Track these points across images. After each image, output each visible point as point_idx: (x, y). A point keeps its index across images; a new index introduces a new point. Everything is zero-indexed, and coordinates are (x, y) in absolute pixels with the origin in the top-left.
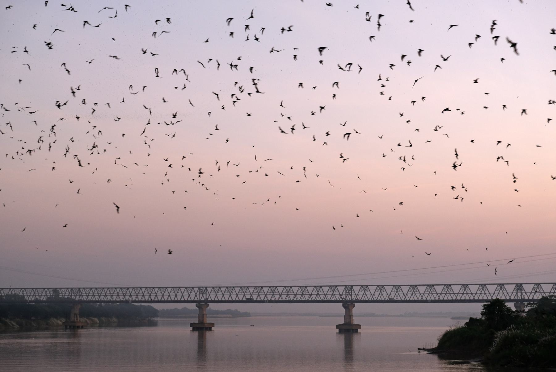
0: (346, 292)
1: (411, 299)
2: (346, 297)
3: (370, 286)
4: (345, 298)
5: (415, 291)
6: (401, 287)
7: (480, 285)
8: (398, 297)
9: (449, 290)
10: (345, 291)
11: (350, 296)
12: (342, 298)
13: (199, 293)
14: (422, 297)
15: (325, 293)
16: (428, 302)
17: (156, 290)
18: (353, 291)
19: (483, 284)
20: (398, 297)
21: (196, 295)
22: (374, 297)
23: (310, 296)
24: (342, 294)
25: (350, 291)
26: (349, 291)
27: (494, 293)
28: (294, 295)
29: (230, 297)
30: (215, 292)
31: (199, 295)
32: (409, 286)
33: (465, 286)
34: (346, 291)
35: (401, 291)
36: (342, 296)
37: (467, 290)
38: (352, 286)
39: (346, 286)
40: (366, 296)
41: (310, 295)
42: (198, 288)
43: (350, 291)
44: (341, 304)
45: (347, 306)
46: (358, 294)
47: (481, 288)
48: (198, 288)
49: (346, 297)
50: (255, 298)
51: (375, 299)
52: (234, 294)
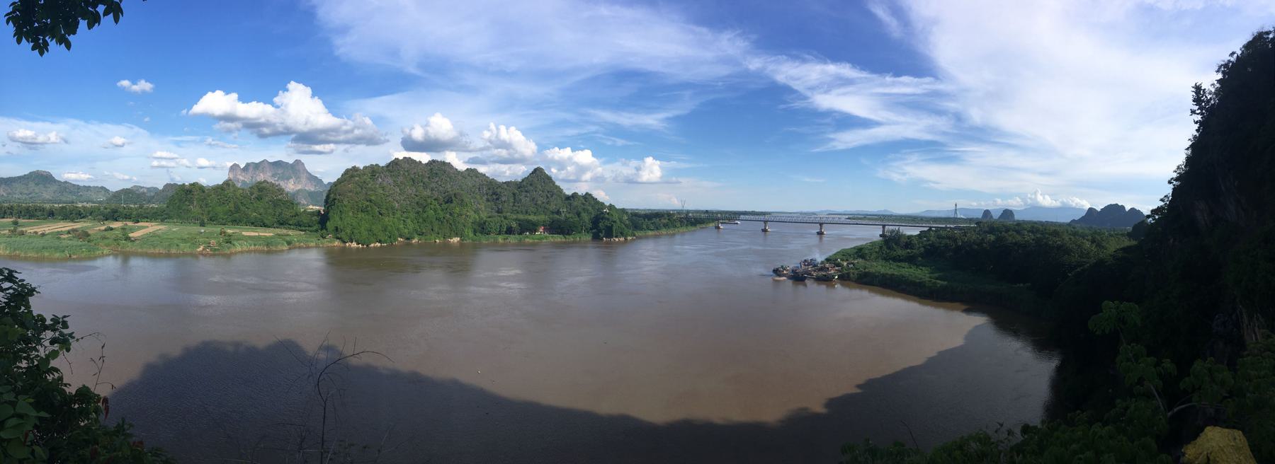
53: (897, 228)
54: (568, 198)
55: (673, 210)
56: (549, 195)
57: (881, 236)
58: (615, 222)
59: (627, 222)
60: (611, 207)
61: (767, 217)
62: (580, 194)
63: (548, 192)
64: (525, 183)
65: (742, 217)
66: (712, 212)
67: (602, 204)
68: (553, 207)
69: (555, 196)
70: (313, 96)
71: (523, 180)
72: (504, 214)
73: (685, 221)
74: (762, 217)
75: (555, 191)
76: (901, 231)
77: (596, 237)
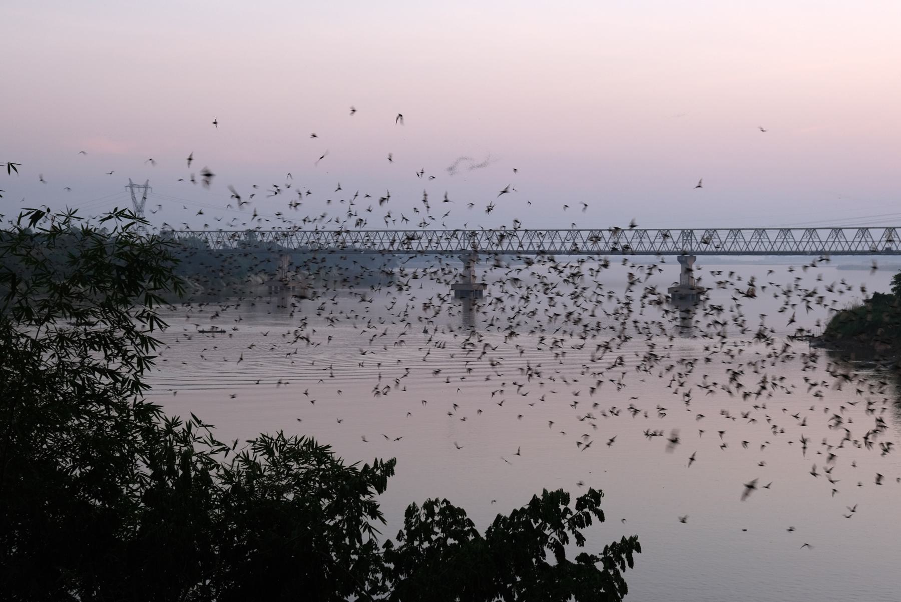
0: (683, 240)
1: (781, 250)
2: (683, 246)
3: (671, 230)
4: (681, 247)
5: (813, 237)
6: (869, 230)
7: (807, 229)
8: (762, 247)
9: (839, 237)
10: (681, 238)
11: (689, 246)
12: (677, 248)
13: (464, 239)
14: (798, 246)
15: (629, 241)
16: (806, 255)
17: (381, 234)
18: (693, 238)
19: (863, 228)
20: (762, 247)
21: (459, 243)
22: (725, 246)
23: (652, 244)
24: (677, 242)
25: (689, 238)
26: (687, 238)
27: (880, 241)
28: (584, 242)
29: (420, 246)
30: (529, 237)
31: (464, 242)
32: (754, 231)
33: (837, 230)
34: (683, 237)
35: (766, 237)
36: (677, 245)
37: (866, 237)
38: (692, 230)
39: (683, 230)
40: (762, 246)
41: (652, 243)
42: (680, 231)
43: (689, 238)
44: (676, 256)
45: (684, 259)
46: (654, 242)
47: (860, 233)
48: (680, 231)
49: (683, 246)
50: (634, 246)
51: (727, 250)
52: (515, 241)
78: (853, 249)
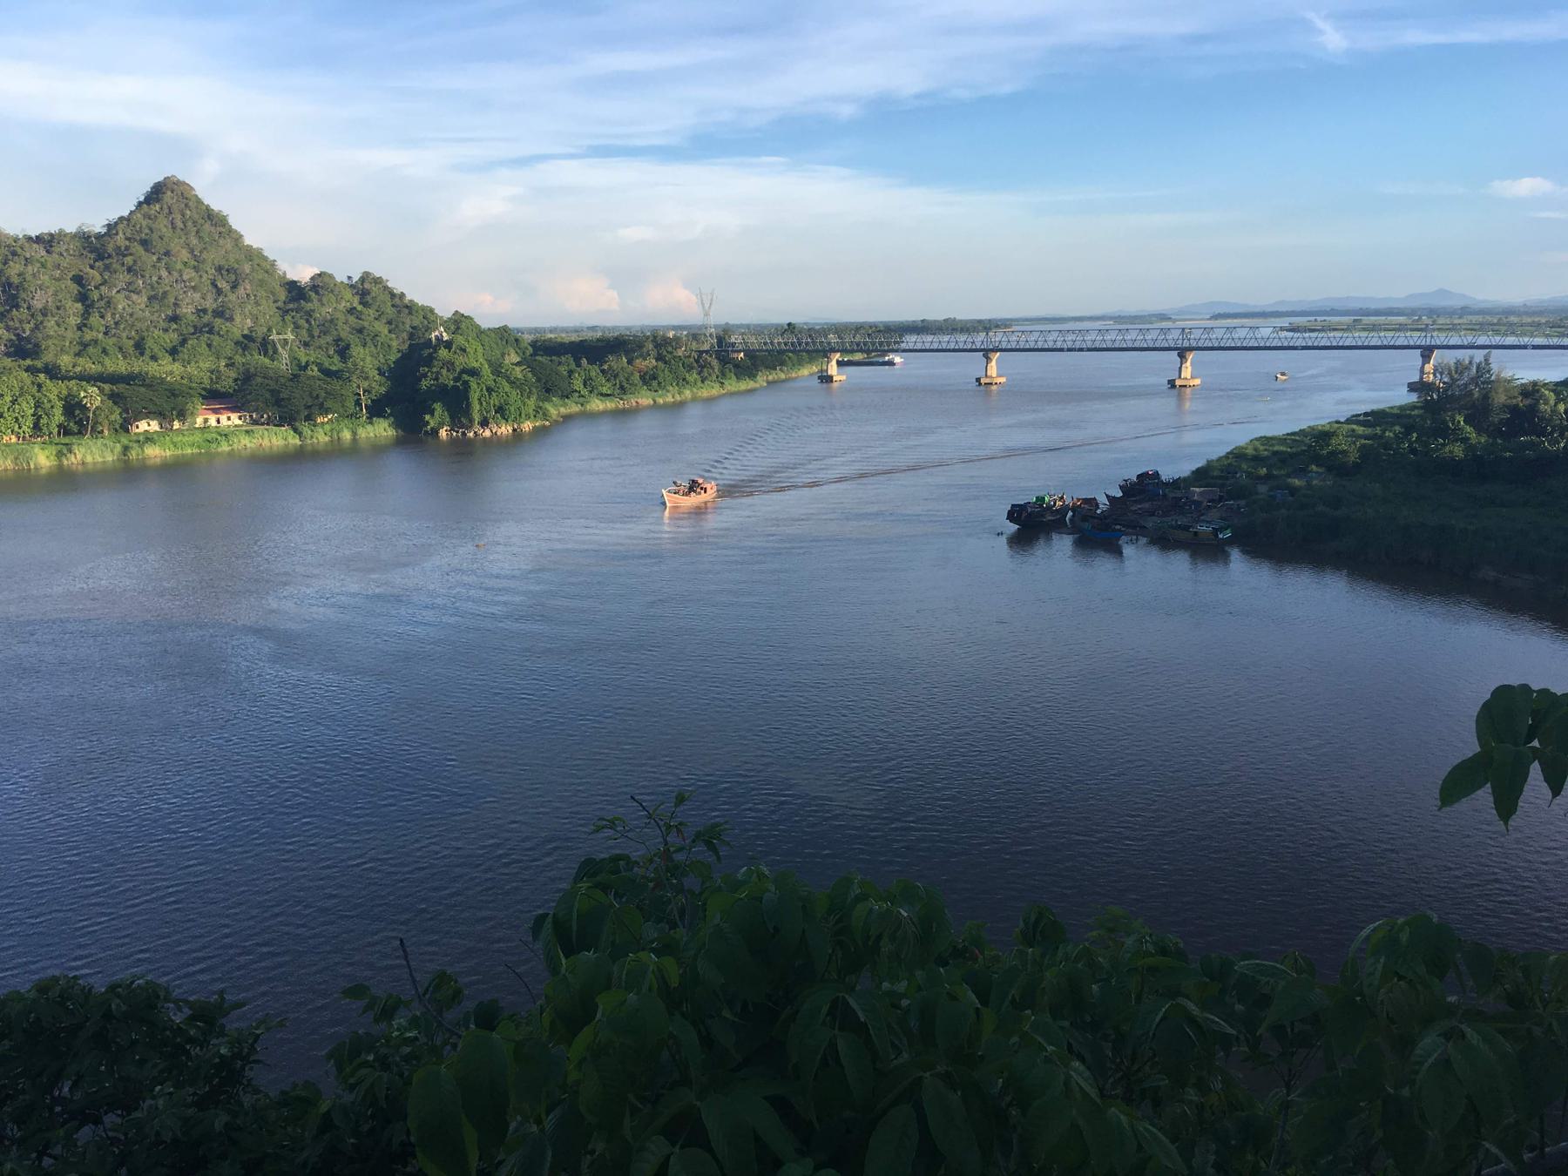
53: (1479, 355)
54: (295, 291)
55: (674, 328)
56: (222, 284)
57: (1412, 387)
58: (474, 373)
59: (518, 372)
60: (459, 322)
61: (997, 337)
62: (341, 277)
63: (219, 269)
64: (120, 239)
65: (911, 340)
66: (811, 331)
67: (428, 313)
68: (242, 324)
69: (246, 288)
70: (1041, 499)
71: (1201, 475)
72: (48, 357)
73: (715, 363)
74: (980, 339)
75: (247, 268)
76: (1494, 367)
77: (413, 432)
78: (1268, 345)
